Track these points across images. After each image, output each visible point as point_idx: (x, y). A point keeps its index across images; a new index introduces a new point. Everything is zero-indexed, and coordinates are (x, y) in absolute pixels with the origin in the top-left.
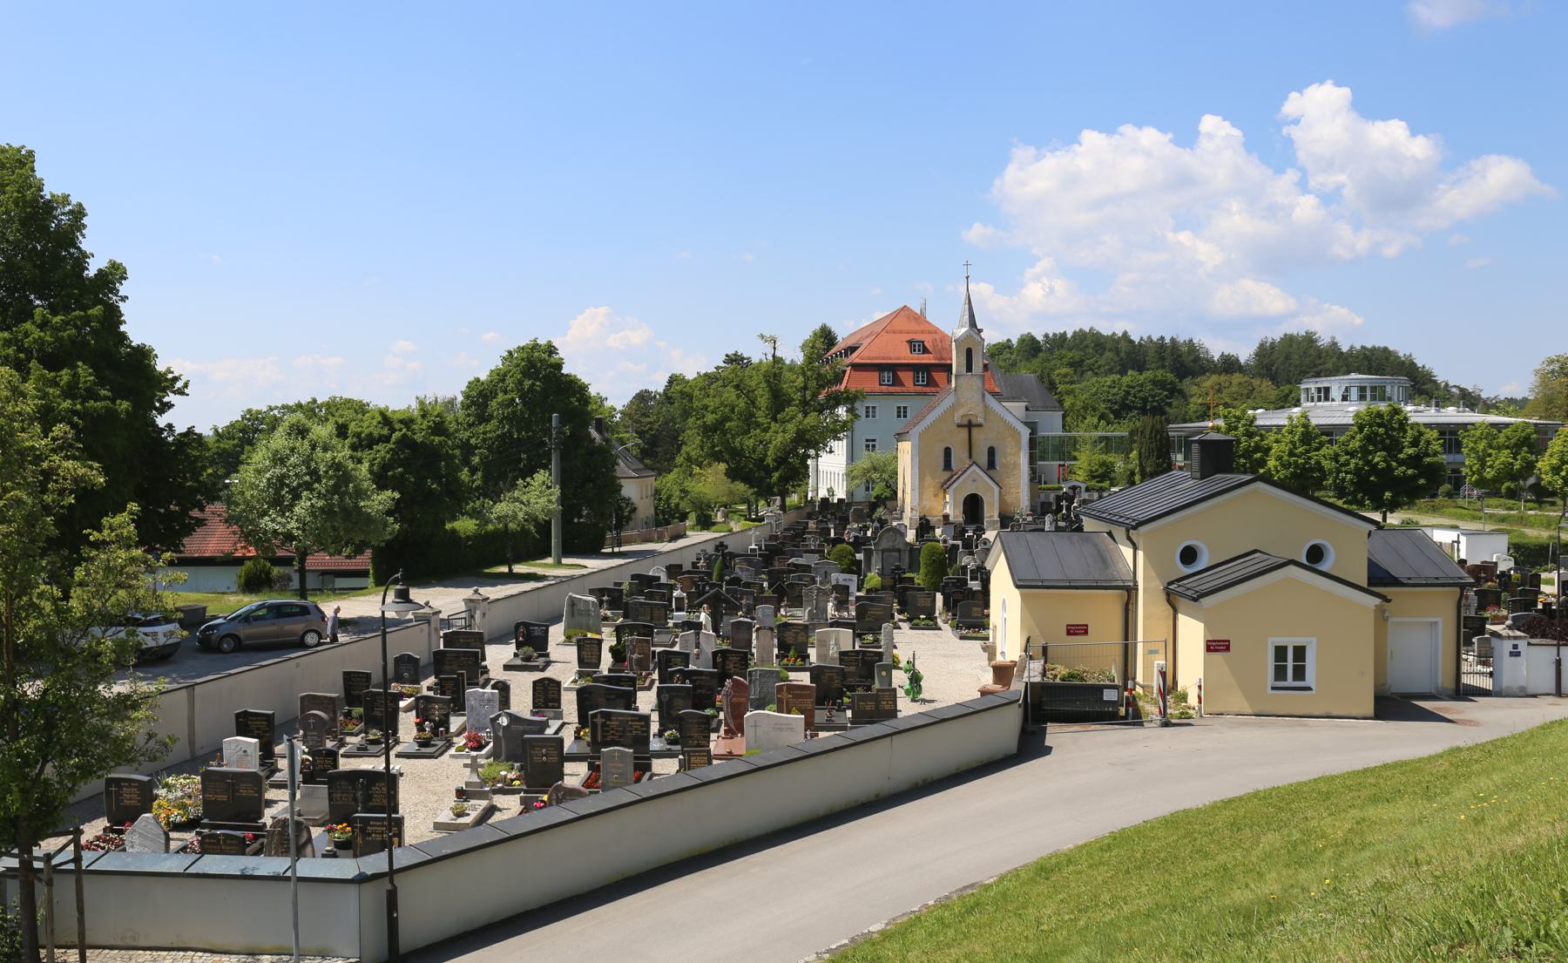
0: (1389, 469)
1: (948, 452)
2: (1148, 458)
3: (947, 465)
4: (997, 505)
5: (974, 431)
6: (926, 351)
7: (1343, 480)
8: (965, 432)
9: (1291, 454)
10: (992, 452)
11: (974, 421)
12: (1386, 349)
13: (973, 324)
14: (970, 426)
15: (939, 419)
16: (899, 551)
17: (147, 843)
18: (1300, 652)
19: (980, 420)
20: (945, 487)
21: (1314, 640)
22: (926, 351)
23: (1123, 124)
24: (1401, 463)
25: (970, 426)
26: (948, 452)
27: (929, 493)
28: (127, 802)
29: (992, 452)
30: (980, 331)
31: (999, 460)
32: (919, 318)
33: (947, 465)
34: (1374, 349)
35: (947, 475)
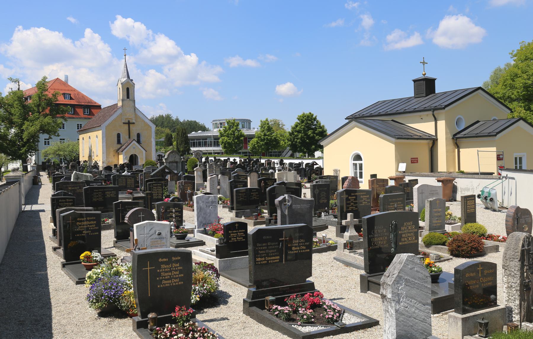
0: (314, 137)
1: (119, 136)
2: (181, 144)
3: (119, 142)
4: (144, 159)
5: (131, 125)
6: (71, 99)
7: (296, 142)
8: (126, 126)
9: (265, 135)
10: (138, 135)
11: (131, 121)
12: (195, 122)
13: (128, 77)
14: (129, 123)
15: (115, 120)
16: (177, 162)
17: (414, 292)
18: (521, 159)
19: (134, 121)
20: (118, 152)
21: (525, 154)
22: (71, 99)
23: (119, 14)
24: (317, 134)
25: (129, 123)
26: (119, 136)
27: (112, 153)
28: (166, 283)
29: (138, 135)
30: (132, 80)
31: (142, 139)
32: (65, 84)
33: (119, 142)
34: (191, 121)
35: (119, 146)
